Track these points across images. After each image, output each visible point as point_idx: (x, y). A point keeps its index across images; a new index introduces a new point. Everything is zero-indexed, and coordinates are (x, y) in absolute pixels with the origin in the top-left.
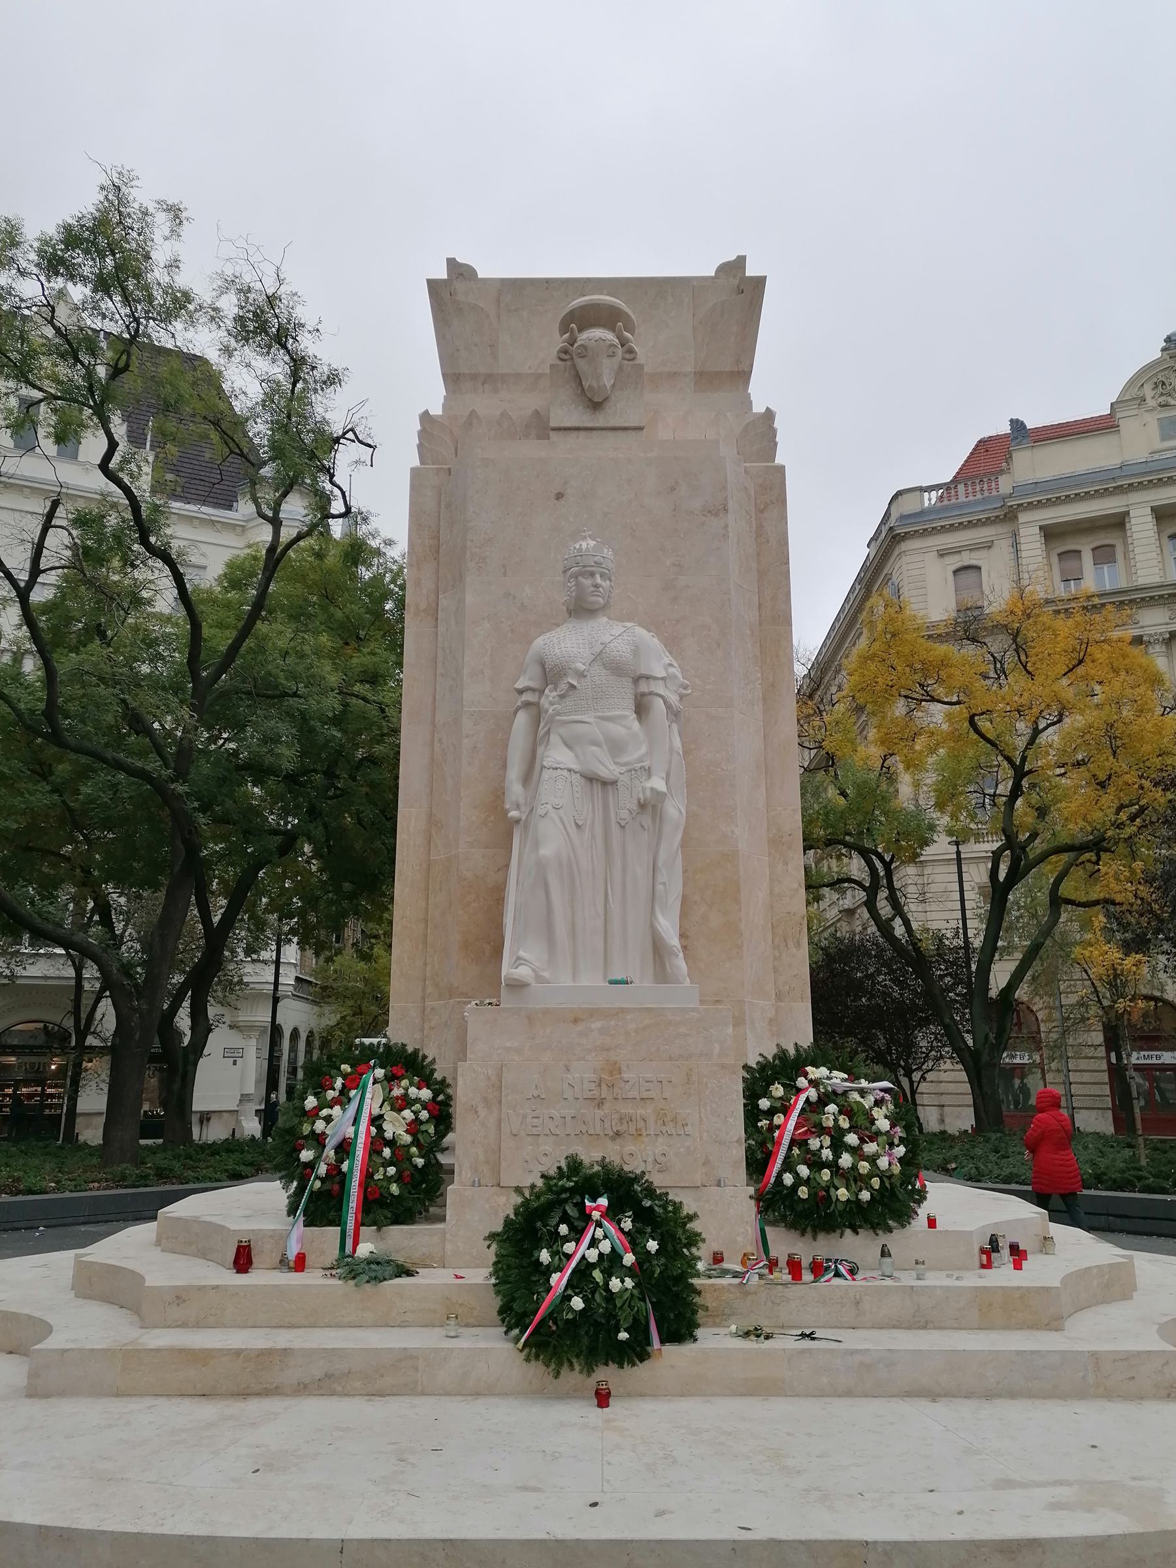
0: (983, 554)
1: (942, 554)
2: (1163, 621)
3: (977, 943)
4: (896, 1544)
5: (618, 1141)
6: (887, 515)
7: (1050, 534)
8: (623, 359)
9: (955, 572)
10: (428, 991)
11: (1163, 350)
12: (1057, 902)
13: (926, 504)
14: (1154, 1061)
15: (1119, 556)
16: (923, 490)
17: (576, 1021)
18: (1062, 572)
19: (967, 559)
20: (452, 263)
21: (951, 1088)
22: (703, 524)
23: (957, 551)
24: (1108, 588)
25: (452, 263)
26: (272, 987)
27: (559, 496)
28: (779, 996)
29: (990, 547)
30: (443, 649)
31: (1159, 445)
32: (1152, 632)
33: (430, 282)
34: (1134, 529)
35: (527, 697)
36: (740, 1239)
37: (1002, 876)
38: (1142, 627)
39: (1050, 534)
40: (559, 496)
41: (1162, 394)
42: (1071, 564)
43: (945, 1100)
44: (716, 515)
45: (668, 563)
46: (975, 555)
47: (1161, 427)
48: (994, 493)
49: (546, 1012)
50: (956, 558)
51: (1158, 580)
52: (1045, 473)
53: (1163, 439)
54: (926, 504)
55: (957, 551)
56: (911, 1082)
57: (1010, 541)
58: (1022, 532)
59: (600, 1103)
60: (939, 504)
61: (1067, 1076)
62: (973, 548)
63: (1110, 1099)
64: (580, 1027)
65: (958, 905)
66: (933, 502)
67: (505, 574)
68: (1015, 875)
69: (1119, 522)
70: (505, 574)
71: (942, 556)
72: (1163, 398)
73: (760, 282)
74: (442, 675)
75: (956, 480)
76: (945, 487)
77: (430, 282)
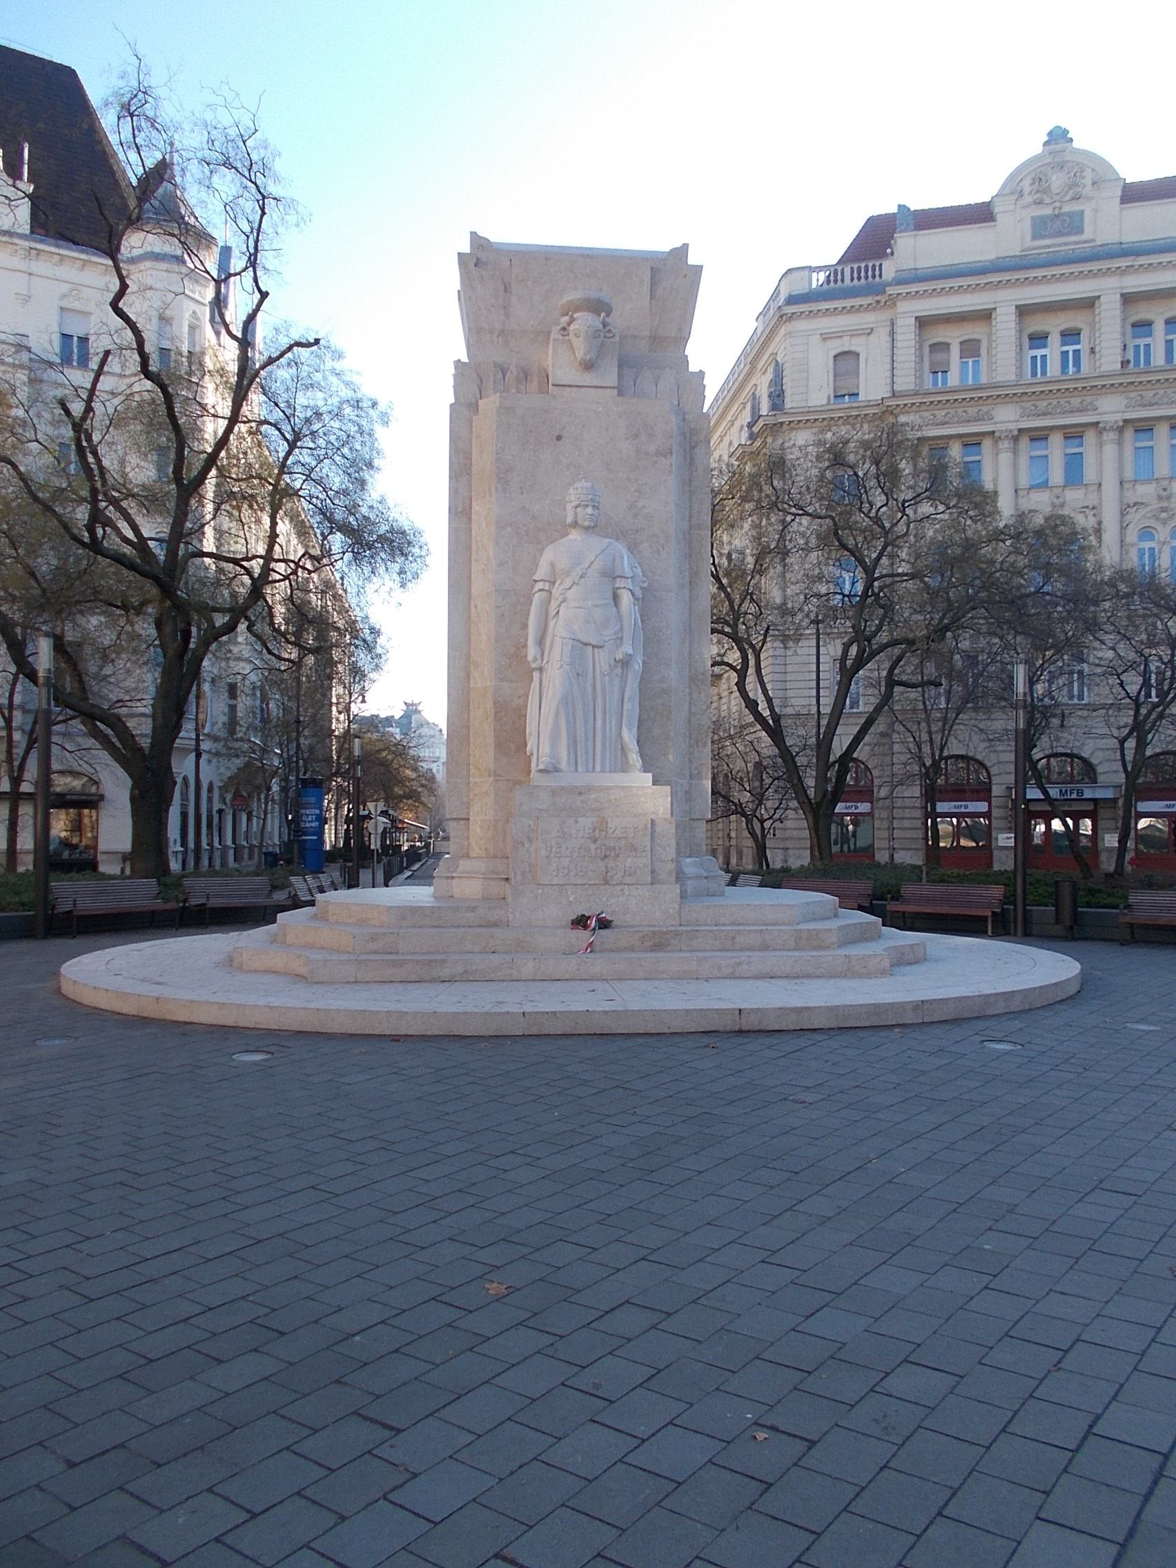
0: (862, 340)
1: (825, 338)
2: (1013, 418)
3: (826, 710)
4: (751, 1009)
5: (606, 860)
6: (777, 291)
7: (923, 323)
8: (605, 337)
9: (835, 357)
10: (471, 772)
11: (1045, 144)
12: (891, 682)
13: (814, 286)
14: (963, 810)
15: (984, 352)
16: (811, 269)
17: (580, 794)
18: (932, 363)
19: (845, 344)
20: (474, 235)
21: (795, 833)
22: (656, 462)
23: (838, 336)
24: (970, 383)
25: (474, 235)
26: (194, 742)
27: (559, 438)
28: (691, 777)
29: (869, 334)
30: (476, 541)
31: (1029, 243)
32: (1004, 428)
33: (459, 254)
34: (999, 326)
35: (540, 585)
36: (671, 911)
37: (849, 663)
38: (996, 423)
39: (923, 323)
40: (559, 438)
41: (1038, 191)
42: (940, 357)
43: (788, 844)
44: (665, 457)
45: (632, 490)
46: (855, 340)
47: (1034, 226)
48: (877, 278)
49: (562, 788)
50: (838, 342)
51: (1013, 377)
52: (925, 263)
53: (1034, 238)
54: (814, 286)
55: (838, 336)
56: (763, 828)
57: (888, 329)
58: (899, 322)
59: (595, 841)
60: (825, 286)
61: (892, 823)
62: (854, 334)
63: (55, 766)
64: (583, 797)
65: (814, 676)
66: (820, 283)
67: (522, 493)
68: (860, 663)
69: (986, 316)
70: (522, 493)
71: (824, 339)
72: (1039, 195)
73: (698, 269)
74: (476, 561)
75: (843, 260)
76: (832, 269)
77: (459, 254)
